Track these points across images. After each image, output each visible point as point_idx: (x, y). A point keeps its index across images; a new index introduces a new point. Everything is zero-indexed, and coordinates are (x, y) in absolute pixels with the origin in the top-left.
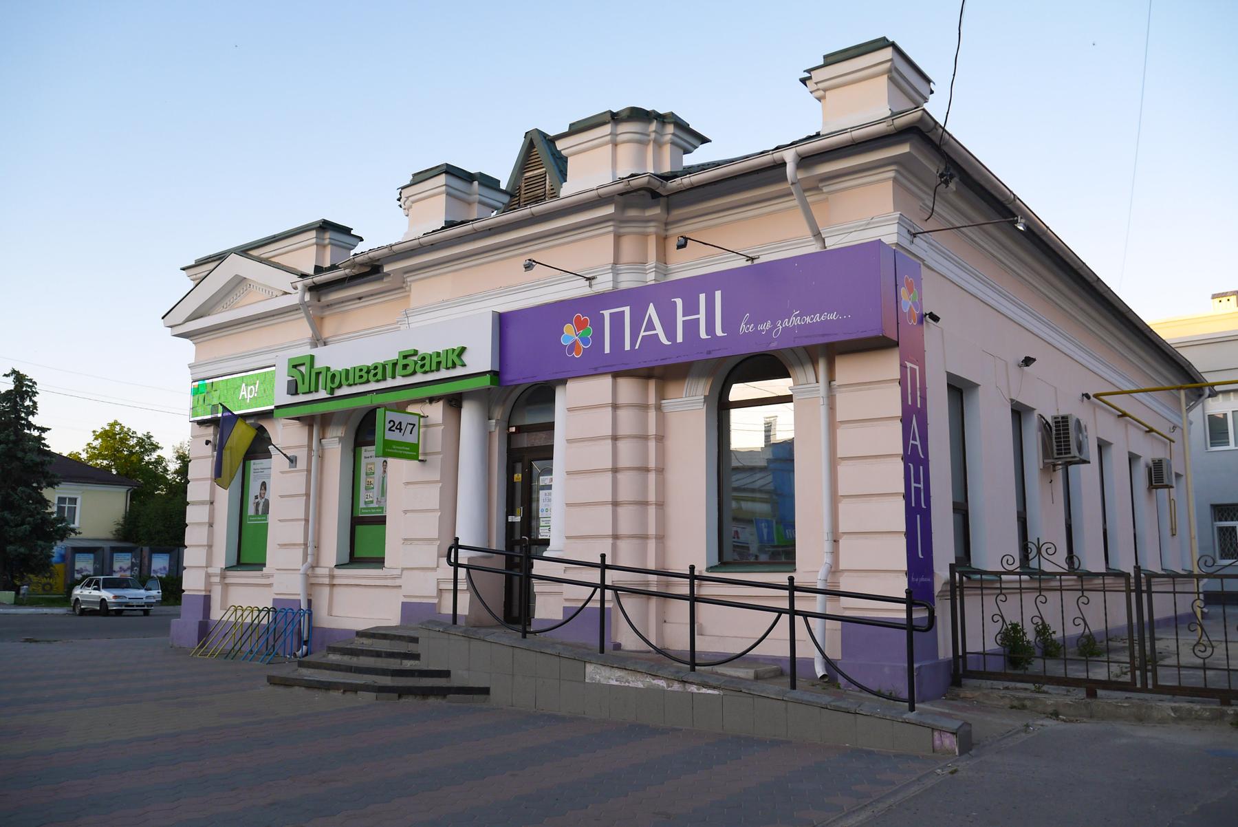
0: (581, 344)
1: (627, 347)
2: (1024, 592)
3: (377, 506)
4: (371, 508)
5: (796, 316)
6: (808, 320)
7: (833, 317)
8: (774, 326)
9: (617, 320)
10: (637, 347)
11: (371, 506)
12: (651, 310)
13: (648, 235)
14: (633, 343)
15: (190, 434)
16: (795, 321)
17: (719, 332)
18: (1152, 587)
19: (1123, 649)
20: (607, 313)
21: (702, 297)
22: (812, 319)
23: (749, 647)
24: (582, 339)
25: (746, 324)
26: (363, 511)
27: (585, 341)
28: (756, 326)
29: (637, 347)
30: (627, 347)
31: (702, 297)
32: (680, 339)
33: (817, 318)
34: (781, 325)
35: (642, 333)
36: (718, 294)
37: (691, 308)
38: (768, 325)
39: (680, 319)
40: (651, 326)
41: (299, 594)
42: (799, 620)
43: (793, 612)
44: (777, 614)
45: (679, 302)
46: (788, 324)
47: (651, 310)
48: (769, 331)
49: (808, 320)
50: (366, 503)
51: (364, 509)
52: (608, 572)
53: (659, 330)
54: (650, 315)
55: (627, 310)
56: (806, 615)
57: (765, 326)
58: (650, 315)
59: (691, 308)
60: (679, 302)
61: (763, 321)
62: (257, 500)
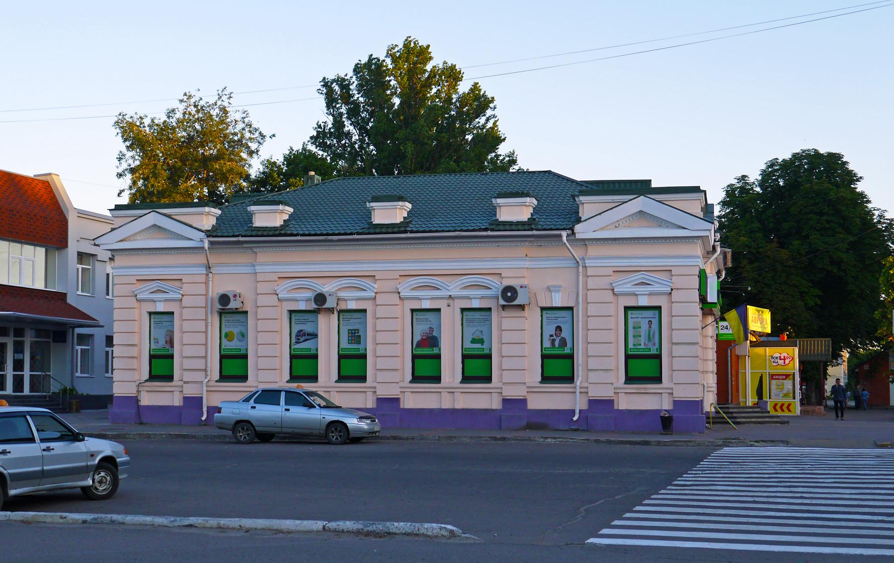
3: (645, 347)
4: (639, 349)
11: (640, 347)
62: (552, 338)
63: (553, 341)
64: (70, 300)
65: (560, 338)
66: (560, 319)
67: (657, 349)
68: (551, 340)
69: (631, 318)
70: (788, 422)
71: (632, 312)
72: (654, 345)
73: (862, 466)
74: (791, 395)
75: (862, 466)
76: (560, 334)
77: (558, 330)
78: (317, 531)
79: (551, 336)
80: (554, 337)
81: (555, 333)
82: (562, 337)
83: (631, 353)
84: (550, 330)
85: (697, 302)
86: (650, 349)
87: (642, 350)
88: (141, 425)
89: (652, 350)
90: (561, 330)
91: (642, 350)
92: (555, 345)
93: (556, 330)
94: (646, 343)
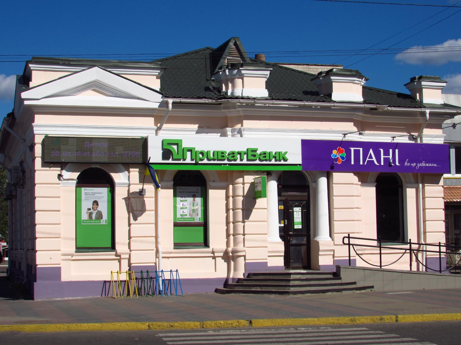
0: (341, 159)
1: (361, 163)
2: (425, 239)
3: (190, 217)
4: (185, 218)
5: (424, 163)
6: (427, 165)
7: (435, 165)
8: (417, 165)
9: (357, 153)
10: (365, 164)
11: (186, 217)
12: (371, 151)
13: (9, 169)
14: (364, 161)
15: (239, 151)
16: (423, 164)
17: (397, 164)
18: (295, 226)
19: (423, 247)
20: (352, 149)
21: (391, 150)
22: (429, 165)
23: (396, 260)
24: (341, 157)
25: (407, 163)
26: (179, 219)
27: (342, 158)
28: (410, 164)
29: (365, 164)
30: (361, 163)
31: (391, 150)
32: (382, 164)
33: (430, 165)
34: (419, 165)
35: (367, 159)
36: (397, 150)
37: (387, 153)
38: (414, 164)
39: (382, 157)
40: (371, 157)
41: (163, 257)
42: (351, 246)
43: (349, 244)
44: (405, 250)
45: (382, 150)
46: (421, 165)
47: (371, 151)
48: (415, 166)
49: (427, 165)
50: (181, 215)
51: (180, 218)
52: (438, 250)
53: (374, 159)
54: (370, 153)
55: (361, 149)
56: (353, 245)
57: (414, 165)
58: (370, 153)
59: (387, 153)
60: (382, 150)
61: (413, 163)
62: (90, 211)
63: (90, 215)
64: (215, 158)
65: (96, 211)
66: (96, 195)
67: (200, 218)
68: (89, 213)
69: (179, 192)
70: (306, 93)
71: (180, 187)
72: (198, 215)
73: (382, 340)
74: (298, 248)
75: (382, 340)
76: (97, 208)
77: (95, 204)
78: (108, 322)
79: (89, 209)
80: (92, 210)
81: (93, 207)
82: (98, 211)
83: (178, 222)
84: (86, 204)
85: (153, 197)
86: (194, 219)
87: (188, 219)
88: (213, 182)
89: (195, 219)
90: (97, 205)
91: (188, 219)
92: (92, 217)
93: (93, 205)
94: (191, 214)
